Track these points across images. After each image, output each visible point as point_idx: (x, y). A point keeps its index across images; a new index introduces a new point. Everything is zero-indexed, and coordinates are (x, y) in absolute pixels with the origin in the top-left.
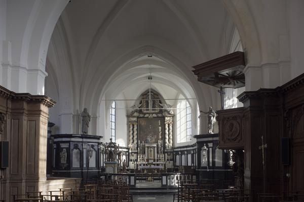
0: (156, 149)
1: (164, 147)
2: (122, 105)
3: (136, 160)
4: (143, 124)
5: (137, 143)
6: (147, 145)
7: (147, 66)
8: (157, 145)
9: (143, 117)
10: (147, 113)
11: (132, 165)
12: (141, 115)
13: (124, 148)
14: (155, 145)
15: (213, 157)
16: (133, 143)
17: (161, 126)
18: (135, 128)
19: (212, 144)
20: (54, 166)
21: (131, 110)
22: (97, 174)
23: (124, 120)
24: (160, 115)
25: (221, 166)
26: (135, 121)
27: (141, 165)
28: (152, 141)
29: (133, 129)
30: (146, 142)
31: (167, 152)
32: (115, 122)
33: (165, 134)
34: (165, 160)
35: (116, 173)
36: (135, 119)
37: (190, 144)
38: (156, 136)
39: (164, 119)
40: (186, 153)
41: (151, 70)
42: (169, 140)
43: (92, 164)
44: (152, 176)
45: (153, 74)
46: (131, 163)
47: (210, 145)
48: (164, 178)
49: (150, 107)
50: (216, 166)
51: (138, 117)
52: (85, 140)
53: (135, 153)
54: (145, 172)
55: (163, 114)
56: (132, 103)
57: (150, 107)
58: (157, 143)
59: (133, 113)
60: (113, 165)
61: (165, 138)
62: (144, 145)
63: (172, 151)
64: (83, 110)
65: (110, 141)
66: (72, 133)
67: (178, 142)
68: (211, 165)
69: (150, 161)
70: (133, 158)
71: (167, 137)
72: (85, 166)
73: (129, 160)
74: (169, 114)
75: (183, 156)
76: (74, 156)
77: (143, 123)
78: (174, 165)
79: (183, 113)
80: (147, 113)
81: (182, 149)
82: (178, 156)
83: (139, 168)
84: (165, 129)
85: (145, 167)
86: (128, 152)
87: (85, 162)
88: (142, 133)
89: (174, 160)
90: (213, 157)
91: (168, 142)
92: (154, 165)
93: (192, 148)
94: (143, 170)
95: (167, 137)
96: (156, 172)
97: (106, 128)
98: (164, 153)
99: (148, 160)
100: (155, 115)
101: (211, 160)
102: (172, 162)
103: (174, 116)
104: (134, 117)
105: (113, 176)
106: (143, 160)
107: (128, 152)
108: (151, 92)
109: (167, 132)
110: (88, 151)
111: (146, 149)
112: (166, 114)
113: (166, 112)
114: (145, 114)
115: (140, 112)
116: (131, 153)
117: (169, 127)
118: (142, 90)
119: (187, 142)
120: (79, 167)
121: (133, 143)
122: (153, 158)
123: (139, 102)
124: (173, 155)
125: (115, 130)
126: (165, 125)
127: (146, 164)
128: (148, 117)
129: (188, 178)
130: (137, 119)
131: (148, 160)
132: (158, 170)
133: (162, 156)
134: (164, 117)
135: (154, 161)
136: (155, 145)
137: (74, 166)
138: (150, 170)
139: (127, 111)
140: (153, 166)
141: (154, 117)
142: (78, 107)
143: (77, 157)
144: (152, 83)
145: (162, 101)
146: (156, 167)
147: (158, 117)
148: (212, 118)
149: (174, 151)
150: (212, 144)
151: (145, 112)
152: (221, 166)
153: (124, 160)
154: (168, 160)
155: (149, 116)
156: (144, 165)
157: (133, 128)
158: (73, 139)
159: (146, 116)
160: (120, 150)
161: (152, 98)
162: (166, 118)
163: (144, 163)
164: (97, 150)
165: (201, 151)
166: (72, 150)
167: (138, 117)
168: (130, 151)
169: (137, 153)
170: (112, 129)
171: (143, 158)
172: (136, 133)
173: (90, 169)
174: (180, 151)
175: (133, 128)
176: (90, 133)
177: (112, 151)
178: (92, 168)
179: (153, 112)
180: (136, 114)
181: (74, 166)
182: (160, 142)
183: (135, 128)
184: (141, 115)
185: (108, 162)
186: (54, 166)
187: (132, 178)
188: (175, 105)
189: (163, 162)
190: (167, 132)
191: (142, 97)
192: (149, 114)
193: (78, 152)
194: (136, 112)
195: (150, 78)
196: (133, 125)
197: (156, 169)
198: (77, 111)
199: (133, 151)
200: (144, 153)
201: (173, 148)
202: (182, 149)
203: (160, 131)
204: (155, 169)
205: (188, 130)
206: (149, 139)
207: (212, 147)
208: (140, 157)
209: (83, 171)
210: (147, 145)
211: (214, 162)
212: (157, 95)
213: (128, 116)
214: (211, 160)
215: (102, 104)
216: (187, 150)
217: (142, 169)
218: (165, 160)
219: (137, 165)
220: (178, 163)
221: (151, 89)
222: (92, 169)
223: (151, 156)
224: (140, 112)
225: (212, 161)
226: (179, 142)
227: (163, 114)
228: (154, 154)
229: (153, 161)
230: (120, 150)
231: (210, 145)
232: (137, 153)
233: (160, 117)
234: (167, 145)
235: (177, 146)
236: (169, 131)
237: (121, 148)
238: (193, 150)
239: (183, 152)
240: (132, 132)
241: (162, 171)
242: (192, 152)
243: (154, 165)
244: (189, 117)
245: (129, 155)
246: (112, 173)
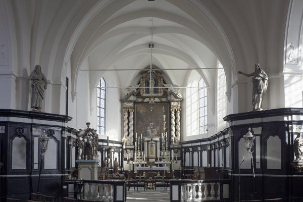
0: (158, 144)
1: (170, 142)
2: (113, 83)
3: (132, 159)
4: (141, 111)
5: (134, 136)
6: (146, 139)
7: (145, 21)
8: (161, 139)
9: (142, 102)
10: (147, 97)
11: (126, 166)
12: (140, 100)
13: (117, 143)
14: (157, 139)
15: (264, 152)
16: (128, 135)
17: (165, 113)
18: (132, 116)
19: (260, 128)
20: (65, 168)
21: (126, 92)
22: (60, 181)
23: (117, 106)
24: (164, 100)
25: (280, 168)
26: (131, 107)
27: (138, 166)
28: (153, 134)
29: (128, 118)
30: (146, 134)
31: (173, 149)
32: (105, 109)
33: (171, 124)
34: (171, 158)
35: (96, 179)
36: (131, 104)
37: (206, 137)
38: (158, 128)
39: (170, 105)
40: (199, 149)
41: (153, 30)
42: (175, 133)
43: (51, 163)
44: (153, 182)
45: (156, 38)
46: (125, 162)
47: (258, 130)
48: (175, 188)
49: (151, 87)
50: (269, 167)
51: (135, 103)
52: (36, 121)
53: (131, 149)
54: (144, 175)
55: (169, 98)
56: (127, 84)
57: (151, 87)
58: (161, 136)
59: (128, 96)
60: (90, 166)
61: (171, 130)
62: (143, 139)
63: (180, 146)
64: (33, 69)
65: (86, 127)
66: (13, 106)
67: (187, 136)
68: (258, 166)
69: (151, 161)
70: (128, 155)
71: (173, 128)
72: (36, 167)
73: (123, 159)
74: (177, 98)
75: (196, 154)
76: (15, 149)
77: (142, 110)
78: (183, 165)
79: (195, 97)
80: (147, 97)
81: (194, 144)
82: (187, 154)
83: (137, 169)
84: (171, 118)
85: (145, 168)
86: (122, 148)
87: (36, 160)
88: (140, 122)
89: (182, 159)
90: (264, 152)
91: (174, 135)
92: (157, 165)
93: (209, 142)
94: (141, 172)
95: (173, 128)
96: (159, 174)
97: (91, 115)
98: (170, 149)
99: (148, 159)
100: (157, 100)
101: (258, 157)
102: (179, 162)
103: (182, 101)
104: (130, 101)
105: (87, 185)
106: (141, 159)
107: (122, 148)
108: (153, 68)
109: (173, 122)
110: (42, 141)
111: (146, 144)
112: (173, 98)
113: (172, 96)
114: (144, 98)
115: (138, 95)
116: (126, 149)
117: (175, 115)
118: (141, 65)
119: (199, 135)
120: (25, 168)
121: (128, 135)
122: (154, 156)
123: (137, 81)
124: (182, 152)
125: (100, 113)
126: (170, 113)
127: (146, 164)
128: (148, 102)
129: (216, 189)
130: (134, 105)
131: (148, 159)
132: (161, 172)
133: (167, 153)
134: (169, 102)
135: (156, 159)
136: (157, 139)
137: (14, 167)
138: (150, 173)
139: (121, 94)
140: (155, 167)
141: (156, 102)
142: (26, 65)
143: (21, 152)
144: (153, 55)
145: (167, 81)
146: (159, 168)
147: (162, 102)
148: (261, 82)
149: (183, 147)
150: (260, 128)
151: (145, 95)
152: (280, 168)
153: (116, 159)
154: (175, 158)
155: (150, 100)
156: (142, 165)
157: (129, 116)
158: (13, 119)
159: (146, 100)
160: (110, 145)
161: (153, 77)
162: (172, 103)
163: (143, 162)
164: (59, 139)
165: (242, 139)
166: (12, 138)
167: (135, 103)
168: (124, 147)
169: (134, 149)
170: (100, 117)
171: (141, 156)
172: (132, 123)
173: (44, 173)
174: (192, 147)
175: (129, 116)
176: (48, 109)
177: (89, 144)
178: (50, 171)
179: (156, 95)
180: (132, 98)
181: (14, 167)
182: (164, 135)
183: (132, 116)
184: (140, 100)
185: (83, 161)
186: (65, 168)
187: (120, 189)
188: (185, 83)
189: (168, 163)
190: (173, 122)
191: (142, 76)
192: (150, 97)
193: (22, 143)
194: (133, 95)
195: (151, 45)
196: (129, 113)
197: (159, 171)
198: (25, 71)
199: (128, 147)
200: (143, 149)
201: (181, 143)
202: (194, 144)
203: (165, 120)
204: (157, 171)
205: (202, 119)
206: (149, 131)
207: (201, 151)
208: (137, 155)
209: (33, 175)
210: (146, 139)
211: (264, 162)
212: (161, 74)
213: (122, 101)
214: (258, 157)
215: (82, 78)
216: (201, 146)
217: (140, 171)
218: (171, 158)
219: (133, 165)
220: (187, 164)
221: (153, 65)
222: (50, 173)
223: (152, 154)
224: (138, 95)
225: (261, 159)
226: (190, 135)
227: (169, 98)
228: (154, 151)
229: (154, 160)
230: (110, 145)
231: (258, 130)
232: (134, 149)
233: (164, 102)
234: (173, 138)
235: (186, 140)
236: (175, 121)
237: (112, 142)
238: (211, 145)
239: (195, 149)
240: (127, 122)
241: (167, 174)
242: (209, 148)
243: (157, 165)
244: (204, 102)
245: (122, 152)
246: (89, 179)
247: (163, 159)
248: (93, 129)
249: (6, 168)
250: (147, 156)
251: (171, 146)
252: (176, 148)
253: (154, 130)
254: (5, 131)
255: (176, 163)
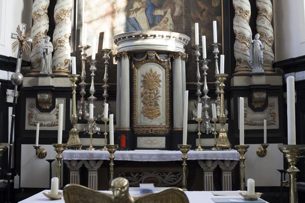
0: (180, 67)
31: (247, 91)
91: (248, 32)
122: (160, 121)
200: (113, 96)
223: (150, 112)
247: (205, 135)
248: (158, 105)
249: (215, 74)
250: (126, 124)
251: (238, 81)
252: (259, 88)
253: (159, 12)
254: (257, 108)
255: (262, 154)
